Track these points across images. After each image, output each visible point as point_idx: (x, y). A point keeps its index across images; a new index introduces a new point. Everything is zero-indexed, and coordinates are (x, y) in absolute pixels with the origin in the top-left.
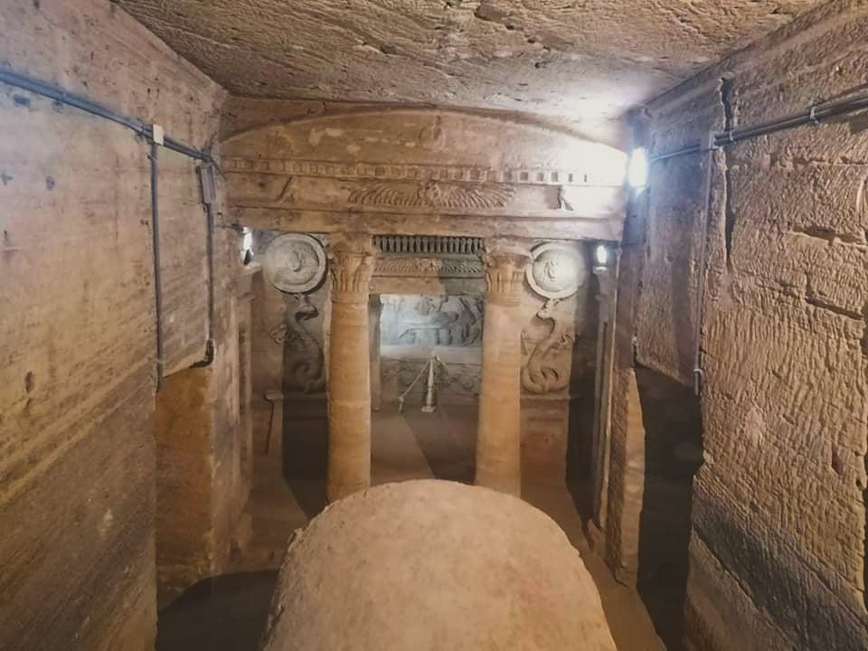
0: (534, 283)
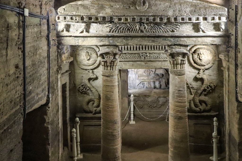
0: (193, 62)
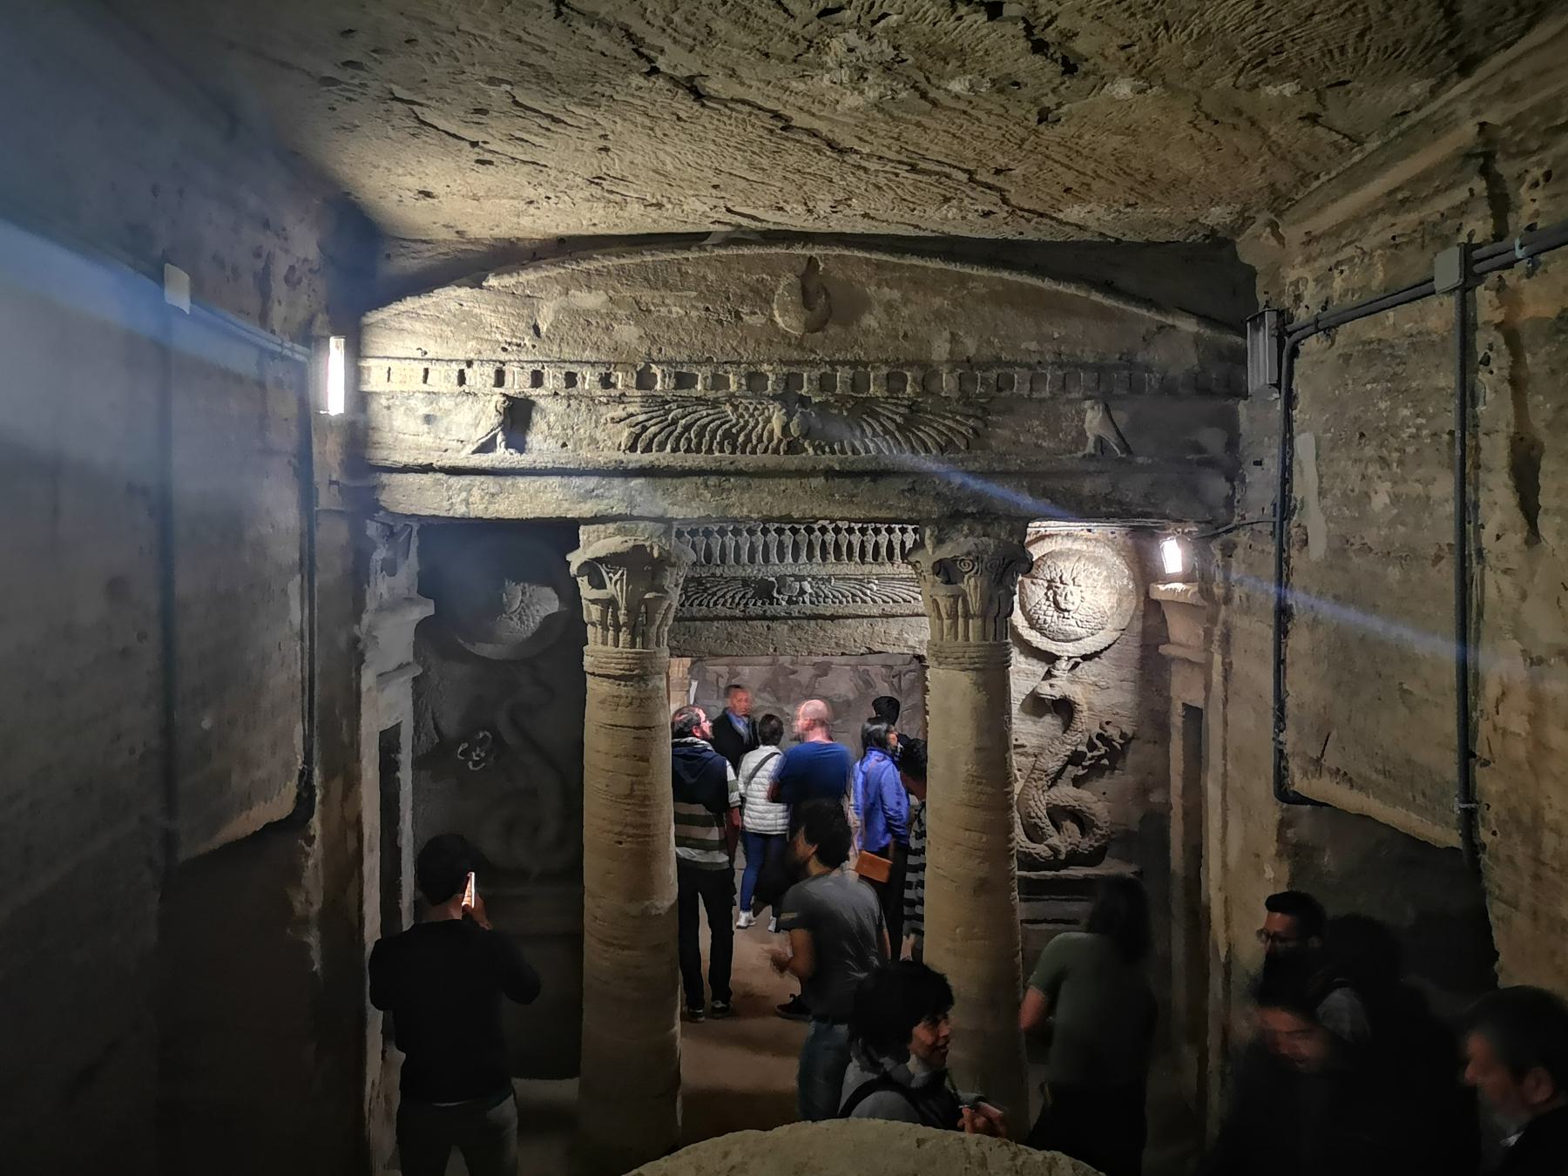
0: (1026, 624)
